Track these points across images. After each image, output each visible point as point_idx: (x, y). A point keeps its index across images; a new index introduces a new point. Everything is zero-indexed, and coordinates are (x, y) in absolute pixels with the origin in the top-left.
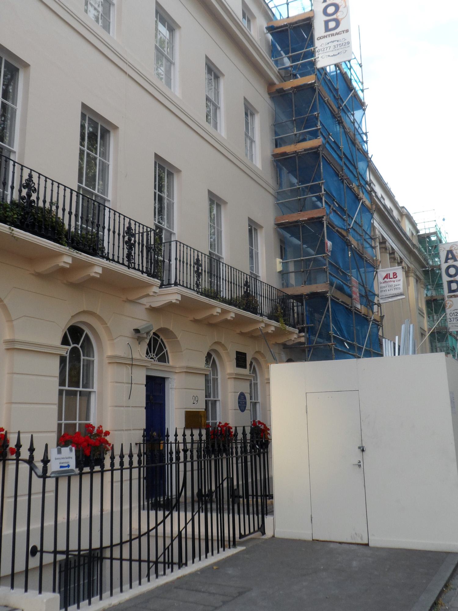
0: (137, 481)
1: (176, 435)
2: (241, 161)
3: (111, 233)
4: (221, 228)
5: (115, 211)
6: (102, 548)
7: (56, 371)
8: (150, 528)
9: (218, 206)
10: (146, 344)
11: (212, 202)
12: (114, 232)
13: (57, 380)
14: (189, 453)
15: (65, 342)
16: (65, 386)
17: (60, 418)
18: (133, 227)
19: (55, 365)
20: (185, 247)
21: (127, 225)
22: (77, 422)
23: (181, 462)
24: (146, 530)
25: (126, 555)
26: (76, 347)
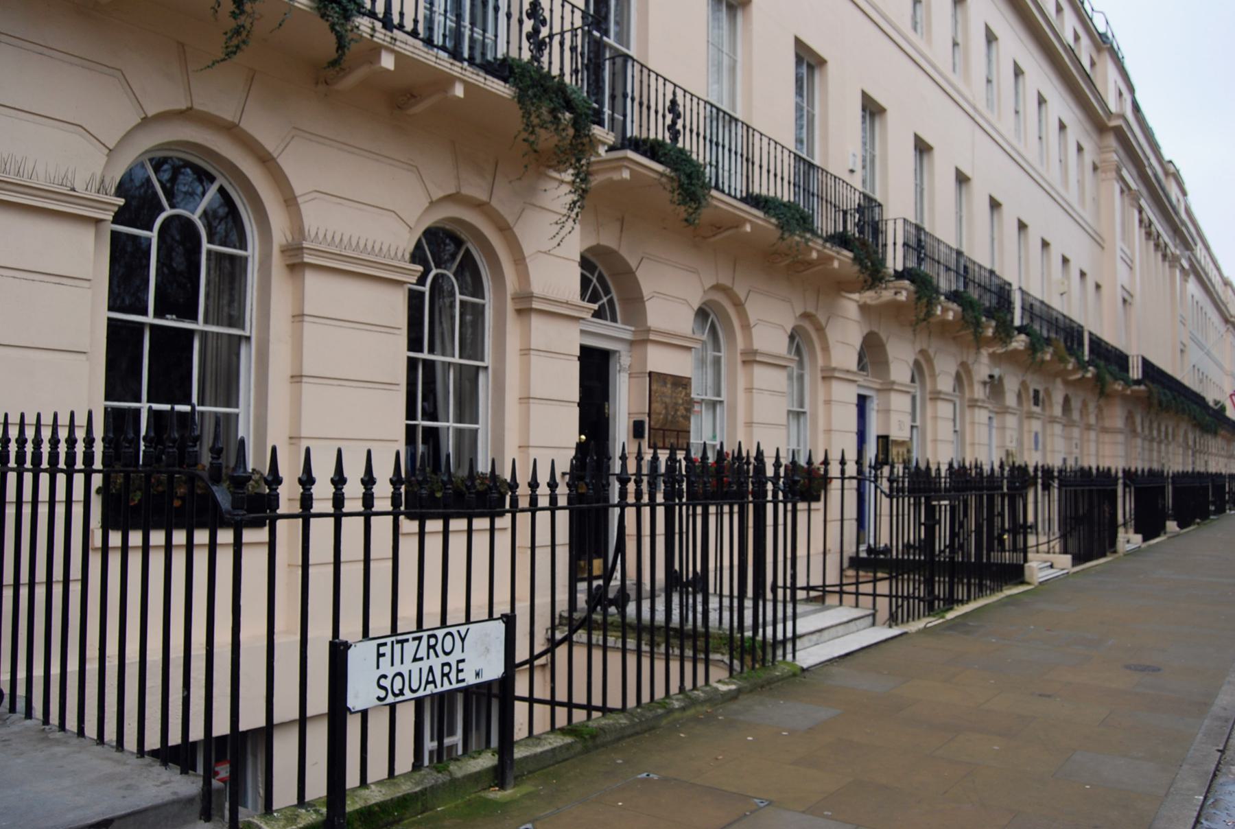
0: (888, 519)
1: (843, 462)
2: (1009, 144)
3: (708, 137)
4: (813, 108)
5: (642, 65)
6: (267, 733)
7: (401, 318)
8: (536, 652)
9: (811, 68)
10: (577, 265)
11: (799, 60)
12: (698, 135)
13: (401, 339)
14: (631, 487)
15: (417, 256)
16: (421, 351)
17: (411, 414)
18: (680, 100)
19: (395, 307)
20: (695, 100)
21: (669, 97)
22: (144, 406)
23: (645, 505)
24: (526, 656)
25: (541, 692)
26: (443, 275)
